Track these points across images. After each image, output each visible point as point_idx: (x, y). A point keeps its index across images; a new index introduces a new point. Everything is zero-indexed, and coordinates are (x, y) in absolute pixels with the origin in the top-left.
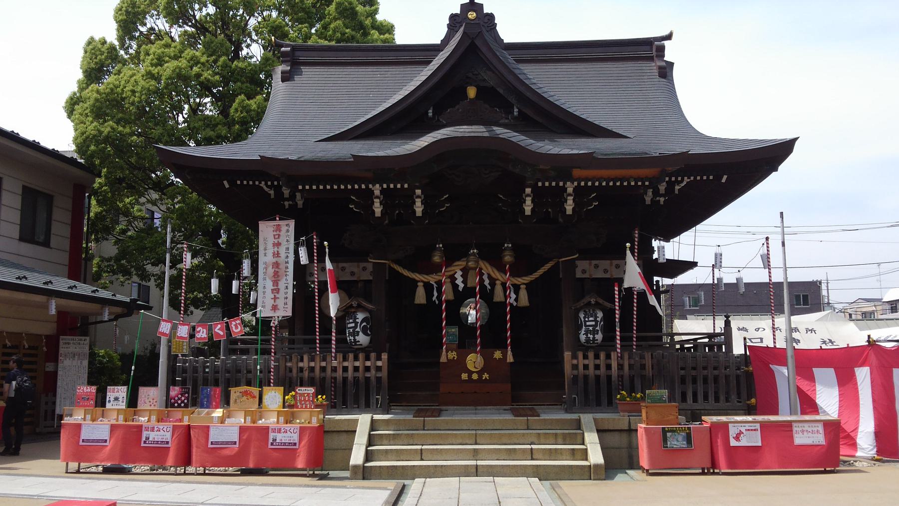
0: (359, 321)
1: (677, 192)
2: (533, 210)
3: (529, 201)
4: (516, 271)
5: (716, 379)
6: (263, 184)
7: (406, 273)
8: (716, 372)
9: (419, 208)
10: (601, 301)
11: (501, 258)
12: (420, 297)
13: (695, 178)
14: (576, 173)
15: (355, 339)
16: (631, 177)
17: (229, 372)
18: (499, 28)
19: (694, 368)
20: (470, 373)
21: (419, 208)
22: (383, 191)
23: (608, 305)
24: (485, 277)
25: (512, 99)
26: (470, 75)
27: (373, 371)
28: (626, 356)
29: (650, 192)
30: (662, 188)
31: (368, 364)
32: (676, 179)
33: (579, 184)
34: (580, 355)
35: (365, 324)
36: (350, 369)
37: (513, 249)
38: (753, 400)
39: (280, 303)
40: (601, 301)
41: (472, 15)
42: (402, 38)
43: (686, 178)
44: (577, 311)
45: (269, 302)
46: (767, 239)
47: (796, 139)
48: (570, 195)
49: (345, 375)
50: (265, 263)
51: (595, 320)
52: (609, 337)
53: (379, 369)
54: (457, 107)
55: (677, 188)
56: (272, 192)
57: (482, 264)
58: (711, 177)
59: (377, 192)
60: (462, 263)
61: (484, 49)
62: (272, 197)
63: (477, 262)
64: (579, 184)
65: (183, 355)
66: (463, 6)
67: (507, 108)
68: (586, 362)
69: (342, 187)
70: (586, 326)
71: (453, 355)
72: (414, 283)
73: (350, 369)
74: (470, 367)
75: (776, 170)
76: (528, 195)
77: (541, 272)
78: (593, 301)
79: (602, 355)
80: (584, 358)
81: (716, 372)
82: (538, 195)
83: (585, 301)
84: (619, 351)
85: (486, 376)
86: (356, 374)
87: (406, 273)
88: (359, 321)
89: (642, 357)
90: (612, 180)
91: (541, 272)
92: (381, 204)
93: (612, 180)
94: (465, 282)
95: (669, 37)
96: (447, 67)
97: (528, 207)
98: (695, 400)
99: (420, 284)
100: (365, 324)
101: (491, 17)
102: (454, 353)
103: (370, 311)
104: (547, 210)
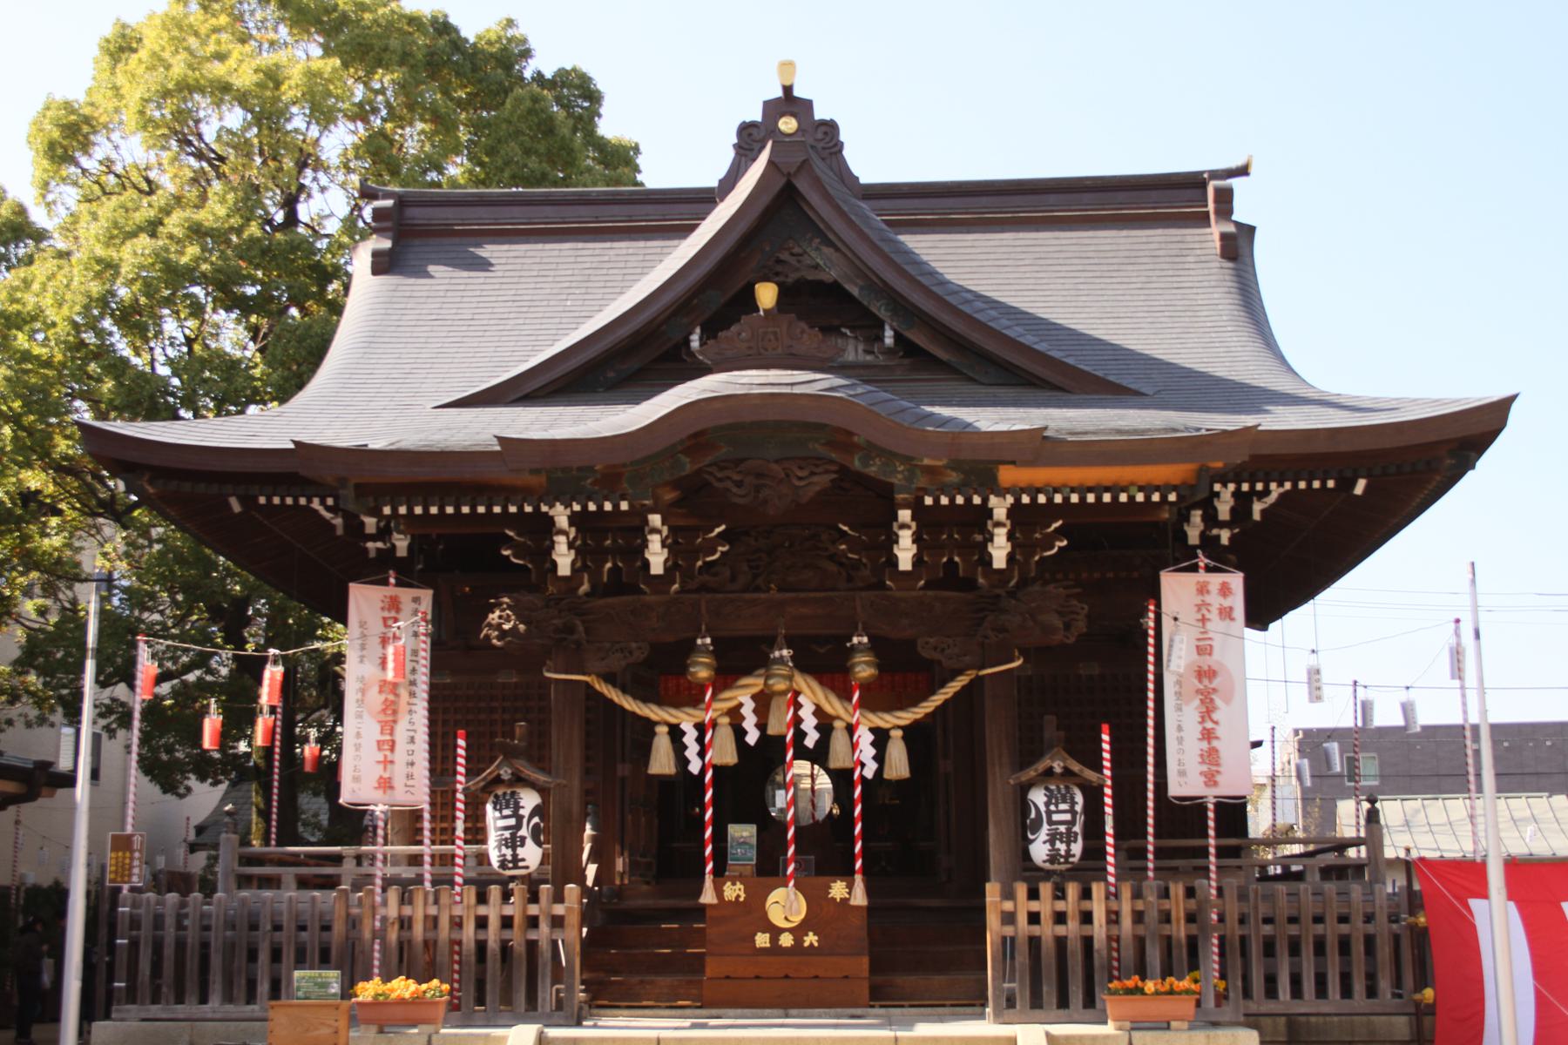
0: (525, 812)
1: (1257, 516)
2: (1011, 558)
3: (655, 542)
4: (874, 699)
5: (1345, 945)
6: (316, 504)
7: (629, 704)
8: (1344, 928)
9: (657, 557)
10: (1076, 767)
11: (847, 671)
12: (661, 762)
13: (1295, 485)
14: (1007, 475)
15: (515, 856)
16: (1132, 484)
17: (233, 928)
18: (847, 153)
19: (1293, 920)
20: (776, 932)
21: (657, 557)
22: (574, 519)
23: (1090, 775)
24: (807, 713)
25: (882, 312)
26: (784, 256)
27: (544, 927)
28: (1126, 893)
29: (1197, 516)
30: (1224, 508)
31: (533, 910)
32: (1252, 487)
33: (1018, 500)
34: (1021, 889)
35: (536, 820)
36: (494, 923)
37: (876, 646)
38: (1429, 993)
39: (399, 772)
40: (1076, 767)
41: (788, 125)
42: (655, 174)
43: (1273, 486)
44: (1025, 788)
45: (374, 772)
46: (1458, 621)
47: (1512, 399)
48: (999, 524)
49: (481, 937)
50: (362, 679)
51: (1072, 811)
52: (1094, 851)
53: (557, 922)
54: (734, 328)
55: (1257, 508)
56: (338, 521)
57: (801, 681)
58: (1331, 484)
59: (562, 521)
60: (755, 683)
61: (814, 198)
62: (340, 532)
63: (790, 678)
64: (1018, 500)
65: (132, 890)
66: (768, 105)
67: (870, 328)
68: (1034, 906)
69: (513, 509)
70: (1050, 822)
71: (733, 891)
72: (649, 726)
73: (494, 923)
74: (776, 916)
75: (1473, 467)
76: (904, 526)
77: (937, 699)
78: (1058, 767)
79: (1072, 890)
80: (1056, 898)
81: (1344, 928)
82: (929, 525)
83: (1041, 766)
84: (1111, 879)
85: (811, 939)
86: (507, 934)
87: (629, 704)
88: (525, 812)
89: (1165, 894)
90: (1157, 488)
91: (937, 699)
92: (664, 545)
93: (1157, 488)
94: (761, 726)
95: (1243, 171)
96: (735, 236)
97: (905, 552)
98: (1297, 992)
99: (662, 730)
100: (536, 820)
101: (831, 127)
102: (739, 885)
103: (542, 790)
104: (951, 560)
